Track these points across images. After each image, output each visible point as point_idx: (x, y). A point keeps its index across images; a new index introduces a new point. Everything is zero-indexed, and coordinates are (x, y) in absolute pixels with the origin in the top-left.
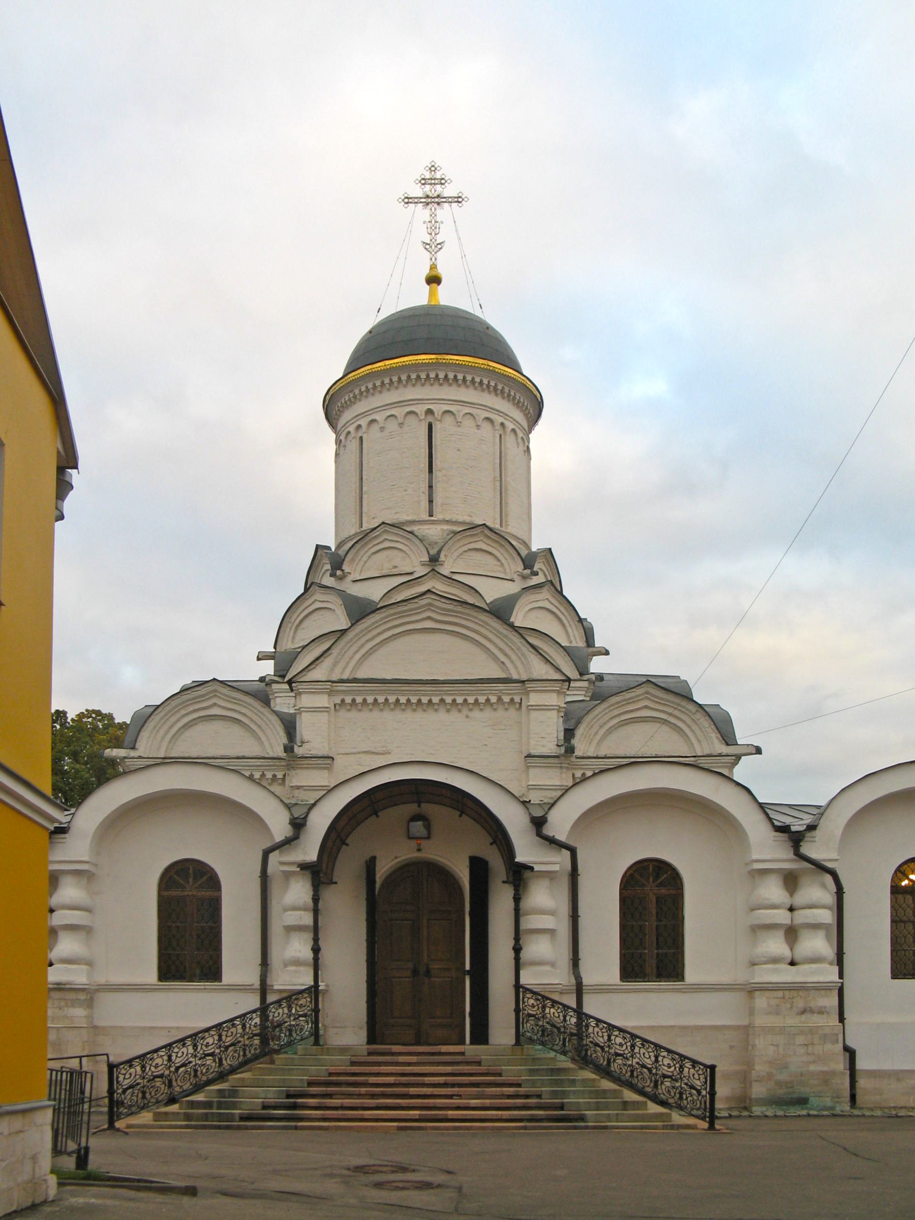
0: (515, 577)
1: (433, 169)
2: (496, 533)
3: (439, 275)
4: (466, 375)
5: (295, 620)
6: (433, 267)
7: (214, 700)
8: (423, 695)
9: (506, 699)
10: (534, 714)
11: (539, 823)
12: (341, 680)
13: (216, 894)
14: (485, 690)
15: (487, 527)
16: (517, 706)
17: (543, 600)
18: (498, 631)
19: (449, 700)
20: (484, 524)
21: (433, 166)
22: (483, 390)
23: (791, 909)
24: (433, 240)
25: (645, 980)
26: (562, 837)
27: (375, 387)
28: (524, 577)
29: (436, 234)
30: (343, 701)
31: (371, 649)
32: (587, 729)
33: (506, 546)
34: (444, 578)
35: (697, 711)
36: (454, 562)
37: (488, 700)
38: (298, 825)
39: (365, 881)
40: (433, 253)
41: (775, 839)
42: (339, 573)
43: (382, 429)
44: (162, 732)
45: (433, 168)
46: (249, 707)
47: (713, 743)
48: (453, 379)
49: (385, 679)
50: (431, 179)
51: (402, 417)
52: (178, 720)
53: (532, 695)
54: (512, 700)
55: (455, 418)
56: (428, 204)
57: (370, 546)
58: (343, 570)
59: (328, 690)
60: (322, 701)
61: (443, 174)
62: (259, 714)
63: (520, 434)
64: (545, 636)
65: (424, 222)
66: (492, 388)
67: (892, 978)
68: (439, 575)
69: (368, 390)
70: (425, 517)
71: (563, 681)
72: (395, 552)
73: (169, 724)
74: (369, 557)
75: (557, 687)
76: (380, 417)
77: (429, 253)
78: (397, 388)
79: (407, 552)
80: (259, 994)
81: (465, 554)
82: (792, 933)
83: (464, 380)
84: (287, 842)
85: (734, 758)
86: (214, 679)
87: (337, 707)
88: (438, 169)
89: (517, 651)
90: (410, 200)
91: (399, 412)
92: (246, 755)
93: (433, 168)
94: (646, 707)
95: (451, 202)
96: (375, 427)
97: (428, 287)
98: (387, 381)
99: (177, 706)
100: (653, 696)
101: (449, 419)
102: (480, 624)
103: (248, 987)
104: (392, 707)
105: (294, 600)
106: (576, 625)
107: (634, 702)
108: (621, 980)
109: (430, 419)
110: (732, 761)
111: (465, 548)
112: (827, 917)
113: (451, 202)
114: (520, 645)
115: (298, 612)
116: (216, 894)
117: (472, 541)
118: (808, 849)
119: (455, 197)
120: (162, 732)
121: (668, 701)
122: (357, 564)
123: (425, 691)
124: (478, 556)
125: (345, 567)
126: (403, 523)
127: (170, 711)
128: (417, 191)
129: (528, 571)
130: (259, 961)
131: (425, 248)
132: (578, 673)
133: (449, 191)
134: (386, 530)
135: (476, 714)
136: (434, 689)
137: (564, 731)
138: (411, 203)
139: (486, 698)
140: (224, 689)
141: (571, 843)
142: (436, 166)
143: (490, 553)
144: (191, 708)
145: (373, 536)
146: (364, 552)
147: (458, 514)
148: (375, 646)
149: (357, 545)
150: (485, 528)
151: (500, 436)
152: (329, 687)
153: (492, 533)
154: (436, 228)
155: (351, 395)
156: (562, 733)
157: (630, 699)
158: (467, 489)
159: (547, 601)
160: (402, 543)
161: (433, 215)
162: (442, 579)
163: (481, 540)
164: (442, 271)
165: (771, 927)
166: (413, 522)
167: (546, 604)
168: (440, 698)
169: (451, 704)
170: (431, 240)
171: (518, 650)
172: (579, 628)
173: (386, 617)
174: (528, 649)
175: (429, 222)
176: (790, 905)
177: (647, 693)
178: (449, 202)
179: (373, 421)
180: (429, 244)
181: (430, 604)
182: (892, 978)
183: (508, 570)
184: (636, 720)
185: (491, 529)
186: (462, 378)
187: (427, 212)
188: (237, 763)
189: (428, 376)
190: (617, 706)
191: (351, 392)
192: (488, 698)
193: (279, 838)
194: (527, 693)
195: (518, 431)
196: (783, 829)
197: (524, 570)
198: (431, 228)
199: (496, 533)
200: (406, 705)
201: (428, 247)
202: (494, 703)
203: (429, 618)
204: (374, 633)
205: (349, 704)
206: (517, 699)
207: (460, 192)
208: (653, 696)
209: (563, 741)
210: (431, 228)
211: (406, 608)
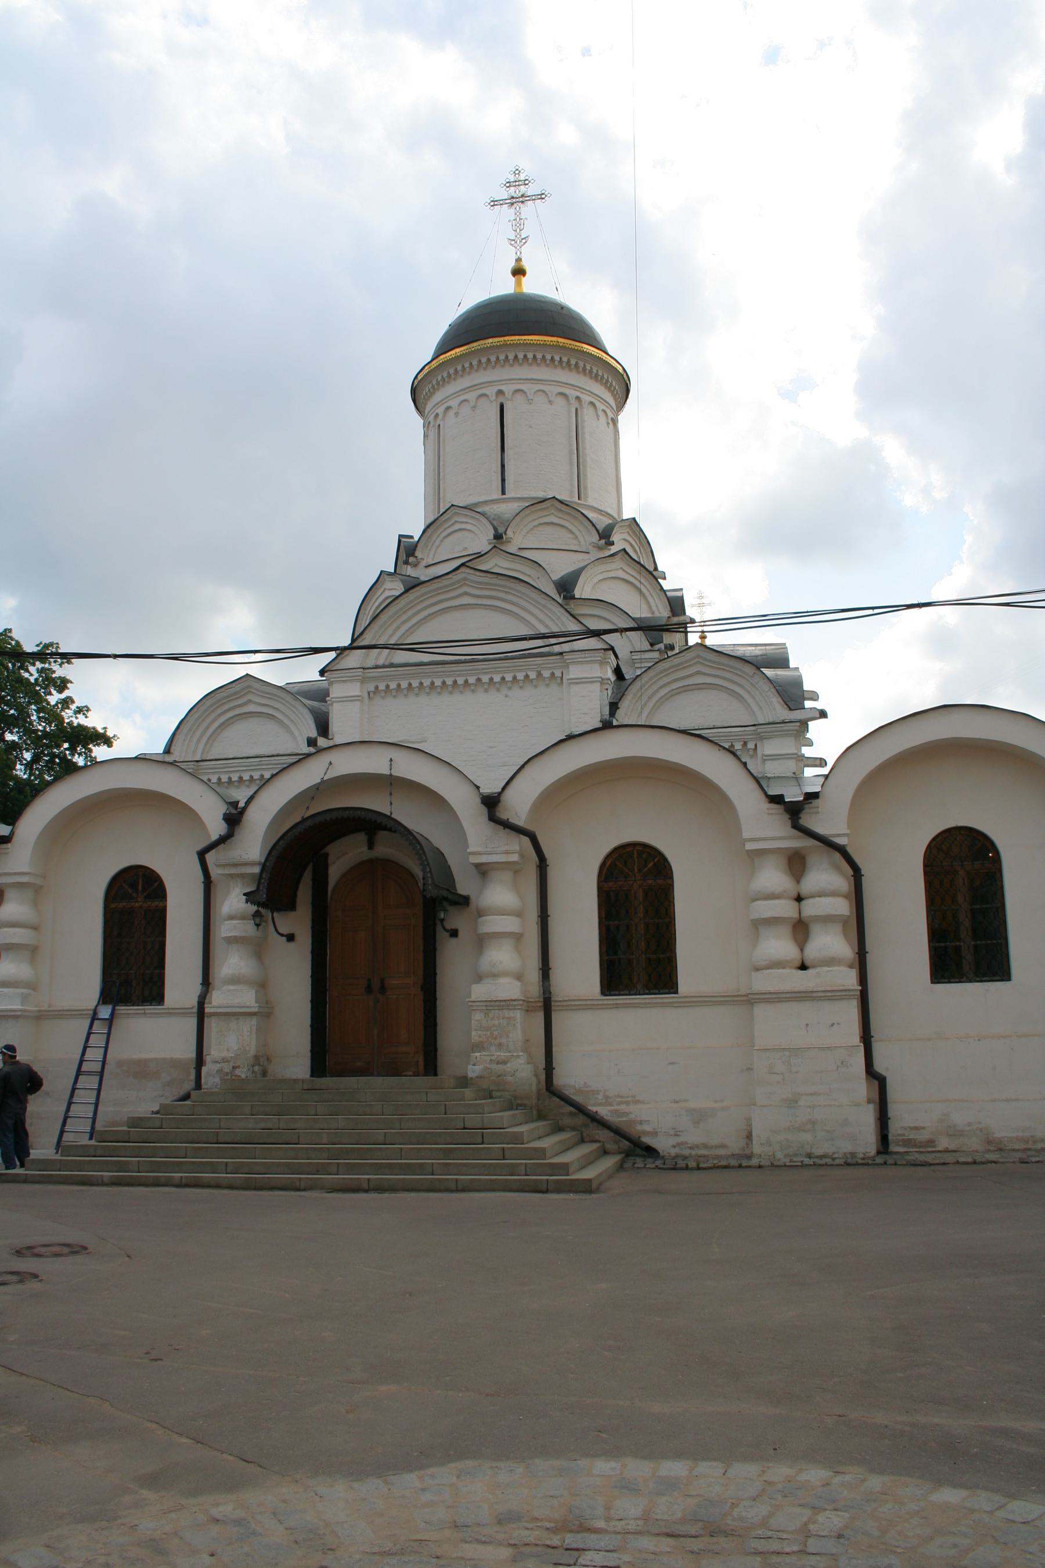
0: (591, 549)
1: (517, 172)
2: (567, 505)
3: (524, 268)
4: (536, 354)
5: (369, 611)
6: (519, 260)
7: (249, 697)
8: (459, 675)
9: (546, 674)
10: (575, 688)
11: (491, 803)
12: (376, 665)
13: (161, 904)
14: (522, 666)
15: (557, 499)
16: (559, 681)
17: (617, 570)
18: (536, 601)
19: (485, 679)
20: (554, 497)
21: (517, 170)
22: (555, 367)
23: (799, 899)
24: (518, 236)
25: (631, 992)
26: (520, 821)
27: (449, 376)
28: (600, 548)
29: (520, 230)
30: (377, 687)
31: (407, 631)
32: (634, 702)
33: (580, 518)
34: (507, 555)
35: (754, 673)
36: (523, 538)
37: (527, 676)
38: (234, 818)
39: (211, 875)
40: (518, 248)
41: (771, 811)
42: (411, 559)
43: (457, 414)
44: (198, 734)
45: (517, 172)
46: (286, 704)
47: (774, 709)
48: (533, 359)
49: (422, 662)
50: (519, 185)
51: (474, 401)
52: (214, 720)
53: (572, 668)
54: (553, 674)
55: (527, 396)
56: (512, 204)
57: (441, 530)
58: (416, 557)
59: (360, 678)
60: (354, 689)
61: (527, 176)
62: (290, 707)
63: (610, 415)
64: (613, 607)
65: (509, 221)
66: (564, 364)
67: (932, 982)
68: (502, 552)
69: (443, 379)
70: (497, 495)
71: (605, 650)
72: (465, 534)
73: (205, 724)
74: (442, 541)
75: (597, 657)
76: (454, 403)
77: (514, 248)
78: (469, 374)
79: (476, 532)
80: (196, 1018)
81: (535, 529)
82: (801, 929)
83: (568, 362)
84: (223, 840)
85: (798, 724)
86: (247, 675)
87: (372, 695)
88: (522, 171)
89: (557, 621)
90: (496, 203)
91: (471, 396)
92: (281, 753)
93: (517, 172)
94: (699, 673)
95: (535, 200)
96: (451, 413)
97: (514, 279)
98: (459, 368)
99: (211, 706)
100: (706, 660)
101: (519, 397)
102: (518, 596)
103: (188, 1011)
104: (428, 690)
105: (367, 590)
106: (658, 594)
107: (685, 668)
108: (603, 993)
109: (501, 399)
110: (797, 728)
111: (536, 523)
112: (843, 907)
113: (535, 200)
114: (559, 614)
115: (373, 600)
116: (161, 904)
117: (543, 515)
118: (807, 821)
119: (538, 195)
120: (198, 734)
121: (723, 665)
122: (430, 550)
123: (460, 671)
124: (549, 530)
125: (418, 553)
126: (477, 504)
127: (206, 711)
128: (504, 194)
129: (603, 541)
130: (200, 980)
131: (511, 244)
132: (648, 644)
133: (531, 190)
134: (455, 513)
135: (516, 692)
136: (468, 668)
137: (610, 706)
138: (497, 205)
139: (525, 674)
140: (256, 684)
141: (530, 827)
142: (520, 169)
143: (563, 526)
144: (227, 707)
145: (444, 519)
146: (436, 536)
147: (531, 490)
148: (411, 628)
149: (429, 530)
150: (556, 501)
151: (576, 410)
152: (360, 673)
153: (562, 505)
154: (520, 225)
155: (430, 386)
156: (608, 708)
157: (679, 665)
158: (541, 465)
159: (621, 570)
160: (471, 524)
161: (518, 213)
162: (505, 556)
163: (552, 514)
164: (526, 264)
165: (773, 921)
166: (486, 503)
167: (621, 574)
168: (476, 677)
169: (489, 684)
170: (516, 236)
171: (558, 620)
172: (661, 597)
173: (422, 595)
174: (567, 618)
175: (514, 220)
176: (797, 894)
177: (698, 656)
178: (533, 200)
179: (448, 408)
180: (514, 240)
181: (465, 579)
182: (932, 982)
183: (583, 542)
184: (691, 687)
185: (561, 502)
186: (574, 363)
187: (512, 210)
188: (269, 762)
189: (498, 358)
190: (665, 673)
191: (429, 383)
192: (527, 674)
193: (214, 837)
194: (567, 666)
195: (597, 403)
196: (777, 800)
197: (599, 540)
198: (516, 225)
199: (567, 505)
200: (442, 688)
201: (513, 242)
202: (534, 679)
203: (466, 594)
204: (410, 613)
205: (383, 690)
206: (558, 674)
207: (543, 190)
208: (706, 660)
209: (608, 716)
210: (516, 225)
211: (440, 585)
